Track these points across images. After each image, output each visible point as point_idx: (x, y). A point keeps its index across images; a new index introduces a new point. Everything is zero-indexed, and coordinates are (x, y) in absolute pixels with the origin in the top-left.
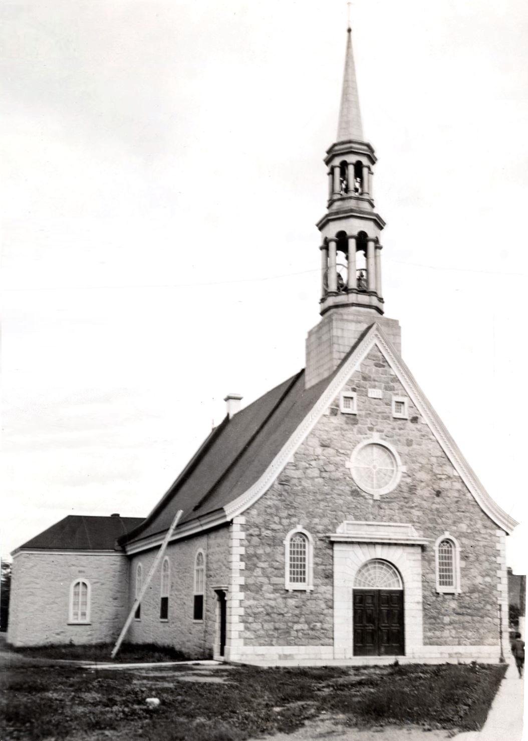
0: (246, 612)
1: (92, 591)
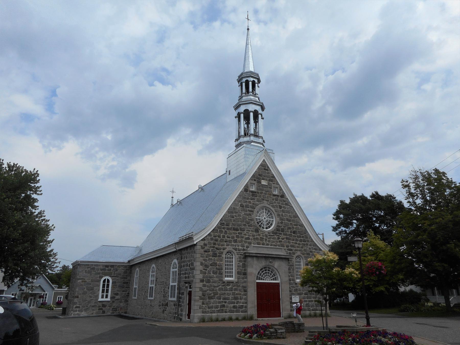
1: (112, 283)
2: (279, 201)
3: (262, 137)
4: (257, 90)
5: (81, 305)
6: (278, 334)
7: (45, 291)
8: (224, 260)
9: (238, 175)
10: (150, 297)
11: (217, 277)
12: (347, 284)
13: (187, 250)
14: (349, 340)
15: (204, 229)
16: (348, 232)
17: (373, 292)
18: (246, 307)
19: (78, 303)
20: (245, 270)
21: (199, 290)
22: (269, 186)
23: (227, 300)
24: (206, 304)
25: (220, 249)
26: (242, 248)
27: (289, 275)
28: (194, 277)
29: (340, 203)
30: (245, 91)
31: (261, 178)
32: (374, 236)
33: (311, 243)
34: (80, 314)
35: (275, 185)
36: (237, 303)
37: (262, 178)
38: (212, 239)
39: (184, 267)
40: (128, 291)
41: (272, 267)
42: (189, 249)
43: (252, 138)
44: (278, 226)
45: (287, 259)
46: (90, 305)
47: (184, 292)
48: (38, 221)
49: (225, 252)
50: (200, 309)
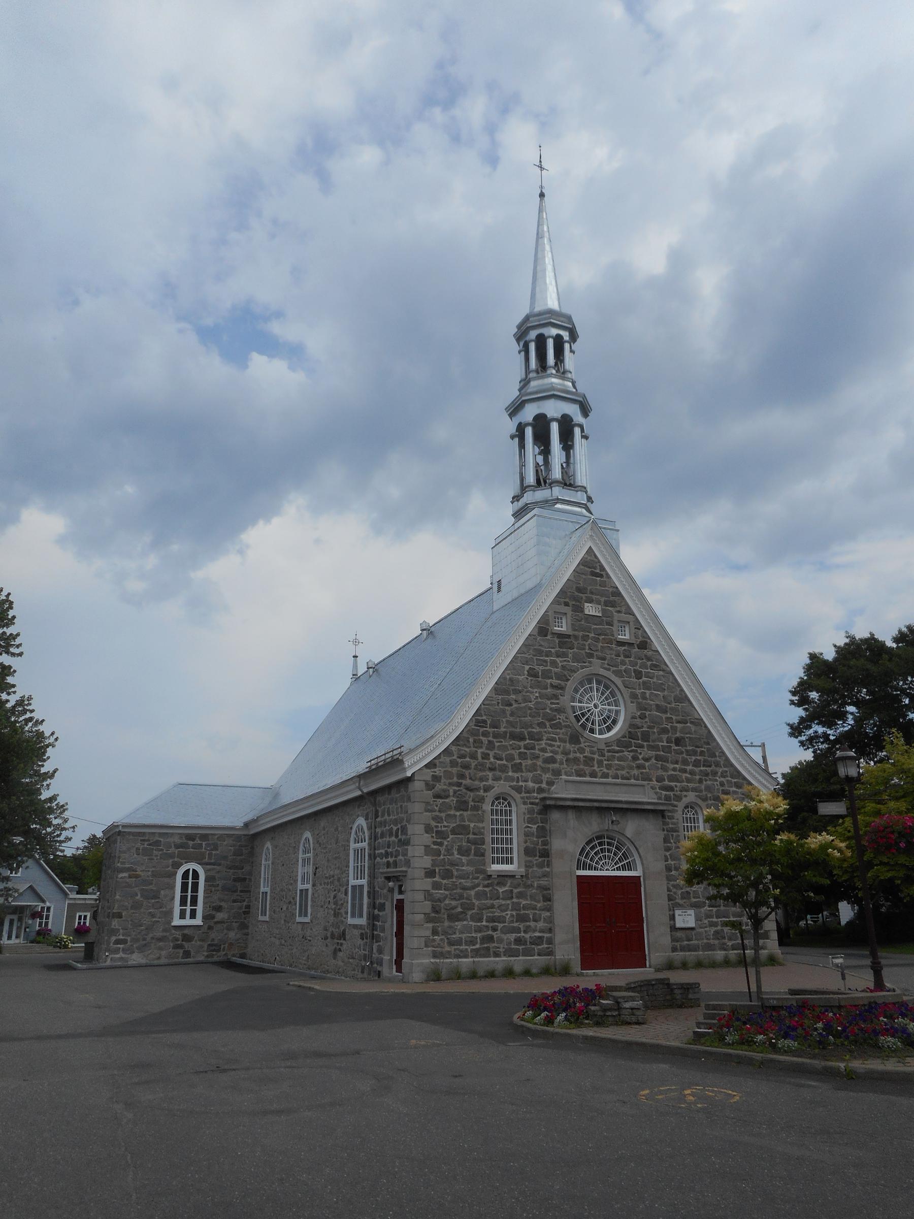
1: (206, 881)
2: (635, 658)
3: (584, 489)
4: (569, 360)
5: (129, 936)
6: (623, 1012)
7: (43, 901)
8: (489, 817)
9: (522, 591)
10: (300, 915)
11: (470, 863)
12: (814, 876)
13: (389, 793)
14: (816, 1029)
15: (432, 737)
16: (832, 738)
17: (904, 897)
18: (550, 941)
19: (121, 931)
20: (545, 843)
21: (423, 897)
22: (606, 620)
23: (499, 922)
24: (442, 935)
25: (478, 789)
26: (537, 786)
27: (666, 856)
28: (408, 863)
29: (808, 659)
30: (536, 365)
31: (584, 598)
32: (905, 747)
33: (725, 769)
34: (127, 958)
35: (623, 616)
36: (525, 932)
37: (586, 597)
38: (453, 764)
39: (383, 838)
40: (247, 900)
41: (617, 836)
42: (394, 791)
43: (557, 491)
44: (632, 726)
45: (661, 814)
46: (151, 935)
47: (384, 904)
48: (16, 722)
49: (490, 796)
50: (426, 946)
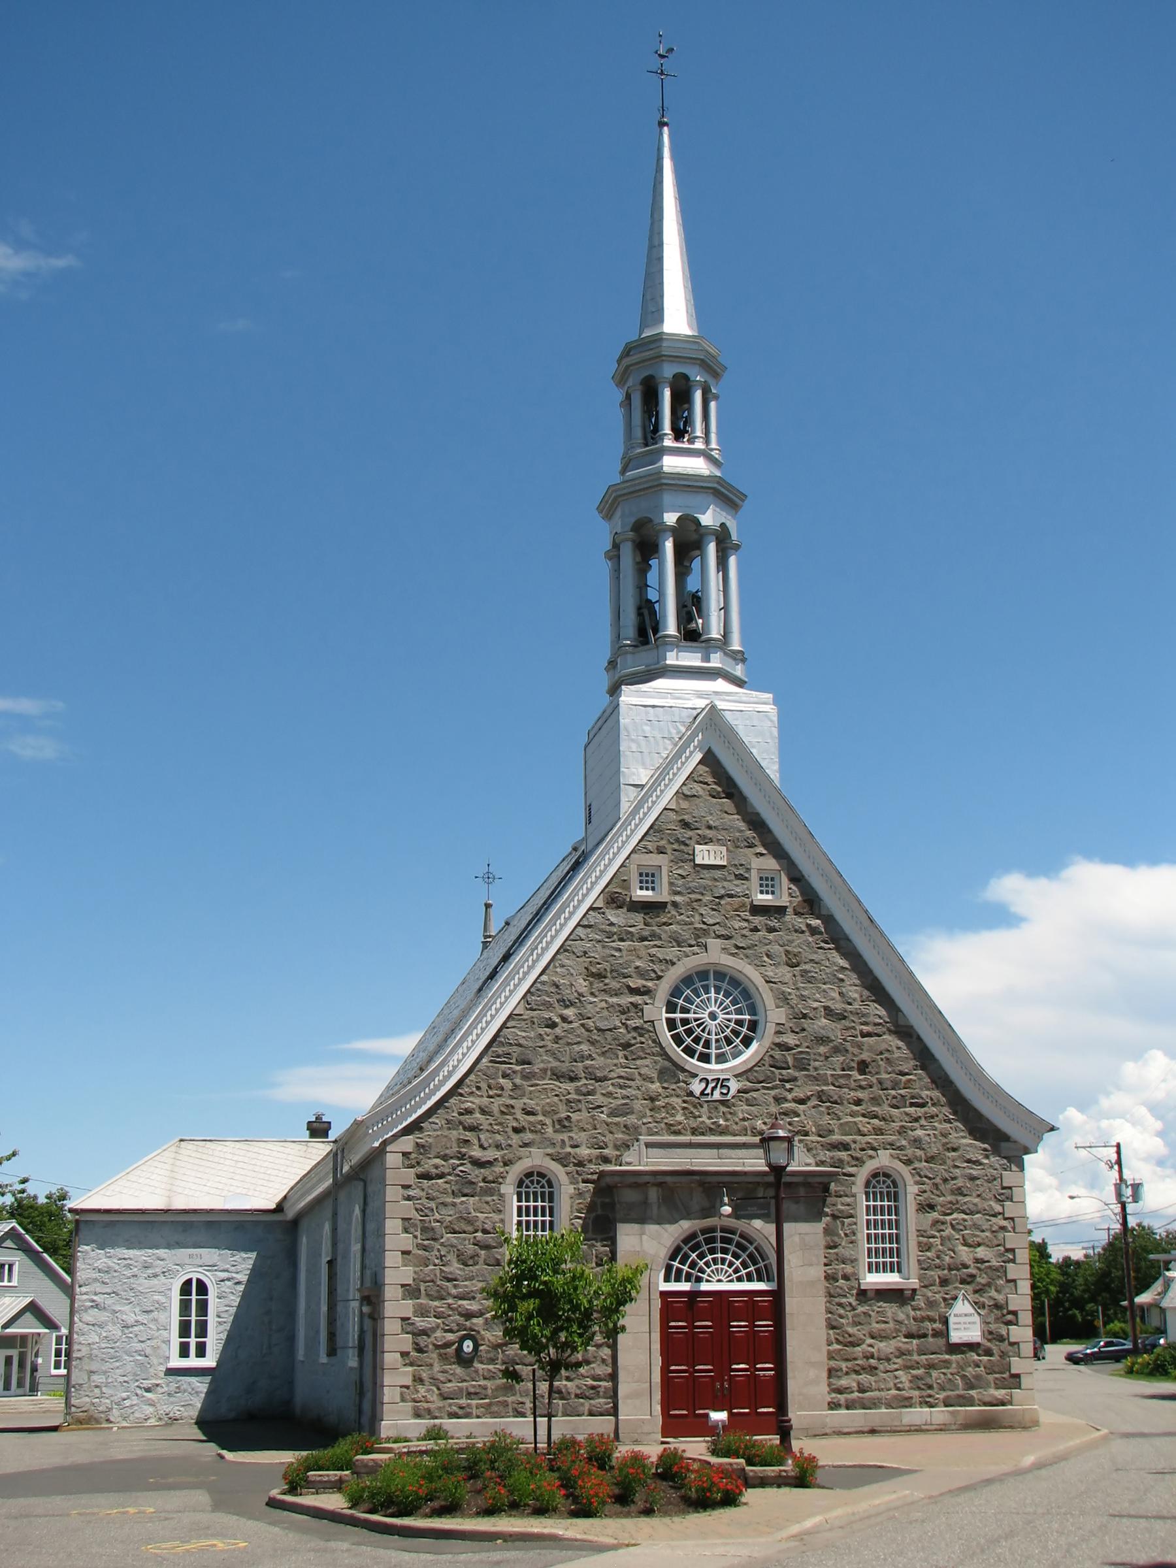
0: (417, 1344)
50: (403, 1400)
